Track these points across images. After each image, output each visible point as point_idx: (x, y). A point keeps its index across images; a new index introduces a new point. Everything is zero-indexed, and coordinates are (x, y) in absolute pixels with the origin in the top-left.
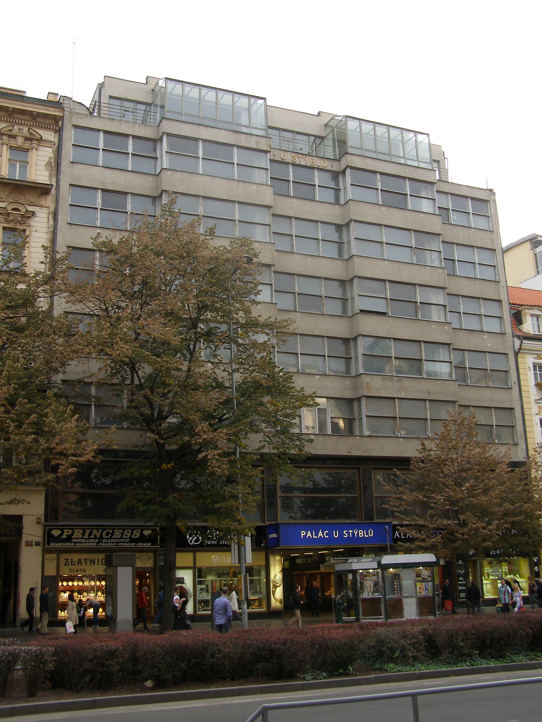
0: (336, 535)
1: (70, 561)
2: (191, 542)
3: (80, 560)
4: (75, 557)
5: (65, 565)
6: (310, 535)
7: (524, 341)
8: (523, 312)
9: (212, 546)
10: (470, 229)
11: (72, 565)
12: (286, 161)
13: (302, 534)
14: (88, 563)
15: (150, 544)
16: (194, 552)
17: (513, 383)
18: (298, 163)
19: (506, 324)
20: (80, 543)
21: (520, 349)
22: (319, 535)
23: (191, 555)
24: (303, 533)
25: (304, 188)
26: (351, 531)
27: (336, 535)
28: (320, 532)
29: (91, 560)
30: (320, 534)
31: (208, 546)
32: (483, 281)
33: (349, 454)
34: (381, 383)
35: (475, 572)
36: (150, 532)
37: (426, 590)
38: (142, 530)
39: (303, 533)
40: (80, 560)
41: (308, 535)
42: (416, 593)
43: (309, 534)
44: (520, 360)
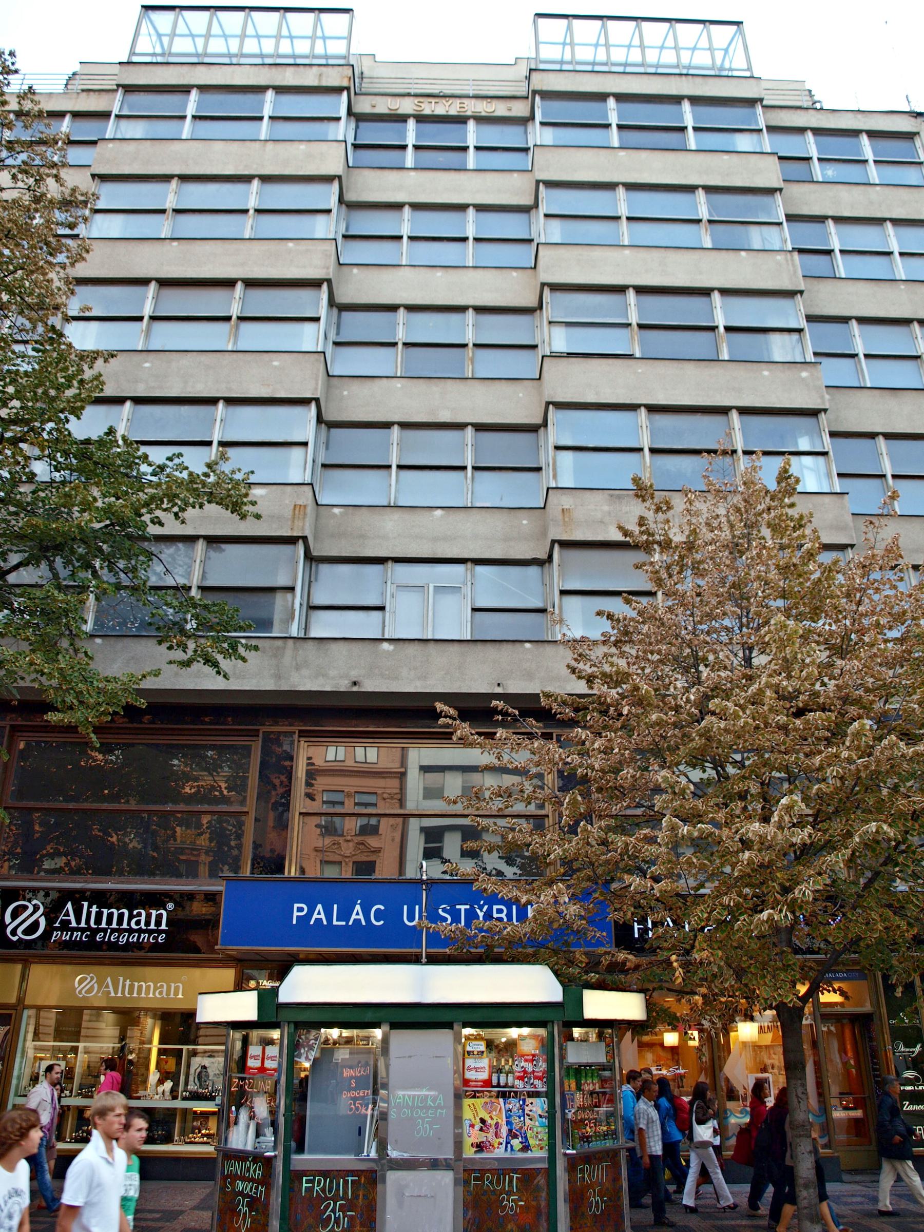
0: (411, 918)
6: (322, 916)
12: (400, 112)
13: (296, 914)
18: (427, 111)
22: (354, 916)
24: (298, 910)
26: (463, 908)
27: (411, 918)
30: (357, 913)
34: (606, 508)
35: (848, 1072)
37: (512, 1134)
39: (300, 910)
41: (315, 916)
42: (458, 1145)
43: (319, 913)
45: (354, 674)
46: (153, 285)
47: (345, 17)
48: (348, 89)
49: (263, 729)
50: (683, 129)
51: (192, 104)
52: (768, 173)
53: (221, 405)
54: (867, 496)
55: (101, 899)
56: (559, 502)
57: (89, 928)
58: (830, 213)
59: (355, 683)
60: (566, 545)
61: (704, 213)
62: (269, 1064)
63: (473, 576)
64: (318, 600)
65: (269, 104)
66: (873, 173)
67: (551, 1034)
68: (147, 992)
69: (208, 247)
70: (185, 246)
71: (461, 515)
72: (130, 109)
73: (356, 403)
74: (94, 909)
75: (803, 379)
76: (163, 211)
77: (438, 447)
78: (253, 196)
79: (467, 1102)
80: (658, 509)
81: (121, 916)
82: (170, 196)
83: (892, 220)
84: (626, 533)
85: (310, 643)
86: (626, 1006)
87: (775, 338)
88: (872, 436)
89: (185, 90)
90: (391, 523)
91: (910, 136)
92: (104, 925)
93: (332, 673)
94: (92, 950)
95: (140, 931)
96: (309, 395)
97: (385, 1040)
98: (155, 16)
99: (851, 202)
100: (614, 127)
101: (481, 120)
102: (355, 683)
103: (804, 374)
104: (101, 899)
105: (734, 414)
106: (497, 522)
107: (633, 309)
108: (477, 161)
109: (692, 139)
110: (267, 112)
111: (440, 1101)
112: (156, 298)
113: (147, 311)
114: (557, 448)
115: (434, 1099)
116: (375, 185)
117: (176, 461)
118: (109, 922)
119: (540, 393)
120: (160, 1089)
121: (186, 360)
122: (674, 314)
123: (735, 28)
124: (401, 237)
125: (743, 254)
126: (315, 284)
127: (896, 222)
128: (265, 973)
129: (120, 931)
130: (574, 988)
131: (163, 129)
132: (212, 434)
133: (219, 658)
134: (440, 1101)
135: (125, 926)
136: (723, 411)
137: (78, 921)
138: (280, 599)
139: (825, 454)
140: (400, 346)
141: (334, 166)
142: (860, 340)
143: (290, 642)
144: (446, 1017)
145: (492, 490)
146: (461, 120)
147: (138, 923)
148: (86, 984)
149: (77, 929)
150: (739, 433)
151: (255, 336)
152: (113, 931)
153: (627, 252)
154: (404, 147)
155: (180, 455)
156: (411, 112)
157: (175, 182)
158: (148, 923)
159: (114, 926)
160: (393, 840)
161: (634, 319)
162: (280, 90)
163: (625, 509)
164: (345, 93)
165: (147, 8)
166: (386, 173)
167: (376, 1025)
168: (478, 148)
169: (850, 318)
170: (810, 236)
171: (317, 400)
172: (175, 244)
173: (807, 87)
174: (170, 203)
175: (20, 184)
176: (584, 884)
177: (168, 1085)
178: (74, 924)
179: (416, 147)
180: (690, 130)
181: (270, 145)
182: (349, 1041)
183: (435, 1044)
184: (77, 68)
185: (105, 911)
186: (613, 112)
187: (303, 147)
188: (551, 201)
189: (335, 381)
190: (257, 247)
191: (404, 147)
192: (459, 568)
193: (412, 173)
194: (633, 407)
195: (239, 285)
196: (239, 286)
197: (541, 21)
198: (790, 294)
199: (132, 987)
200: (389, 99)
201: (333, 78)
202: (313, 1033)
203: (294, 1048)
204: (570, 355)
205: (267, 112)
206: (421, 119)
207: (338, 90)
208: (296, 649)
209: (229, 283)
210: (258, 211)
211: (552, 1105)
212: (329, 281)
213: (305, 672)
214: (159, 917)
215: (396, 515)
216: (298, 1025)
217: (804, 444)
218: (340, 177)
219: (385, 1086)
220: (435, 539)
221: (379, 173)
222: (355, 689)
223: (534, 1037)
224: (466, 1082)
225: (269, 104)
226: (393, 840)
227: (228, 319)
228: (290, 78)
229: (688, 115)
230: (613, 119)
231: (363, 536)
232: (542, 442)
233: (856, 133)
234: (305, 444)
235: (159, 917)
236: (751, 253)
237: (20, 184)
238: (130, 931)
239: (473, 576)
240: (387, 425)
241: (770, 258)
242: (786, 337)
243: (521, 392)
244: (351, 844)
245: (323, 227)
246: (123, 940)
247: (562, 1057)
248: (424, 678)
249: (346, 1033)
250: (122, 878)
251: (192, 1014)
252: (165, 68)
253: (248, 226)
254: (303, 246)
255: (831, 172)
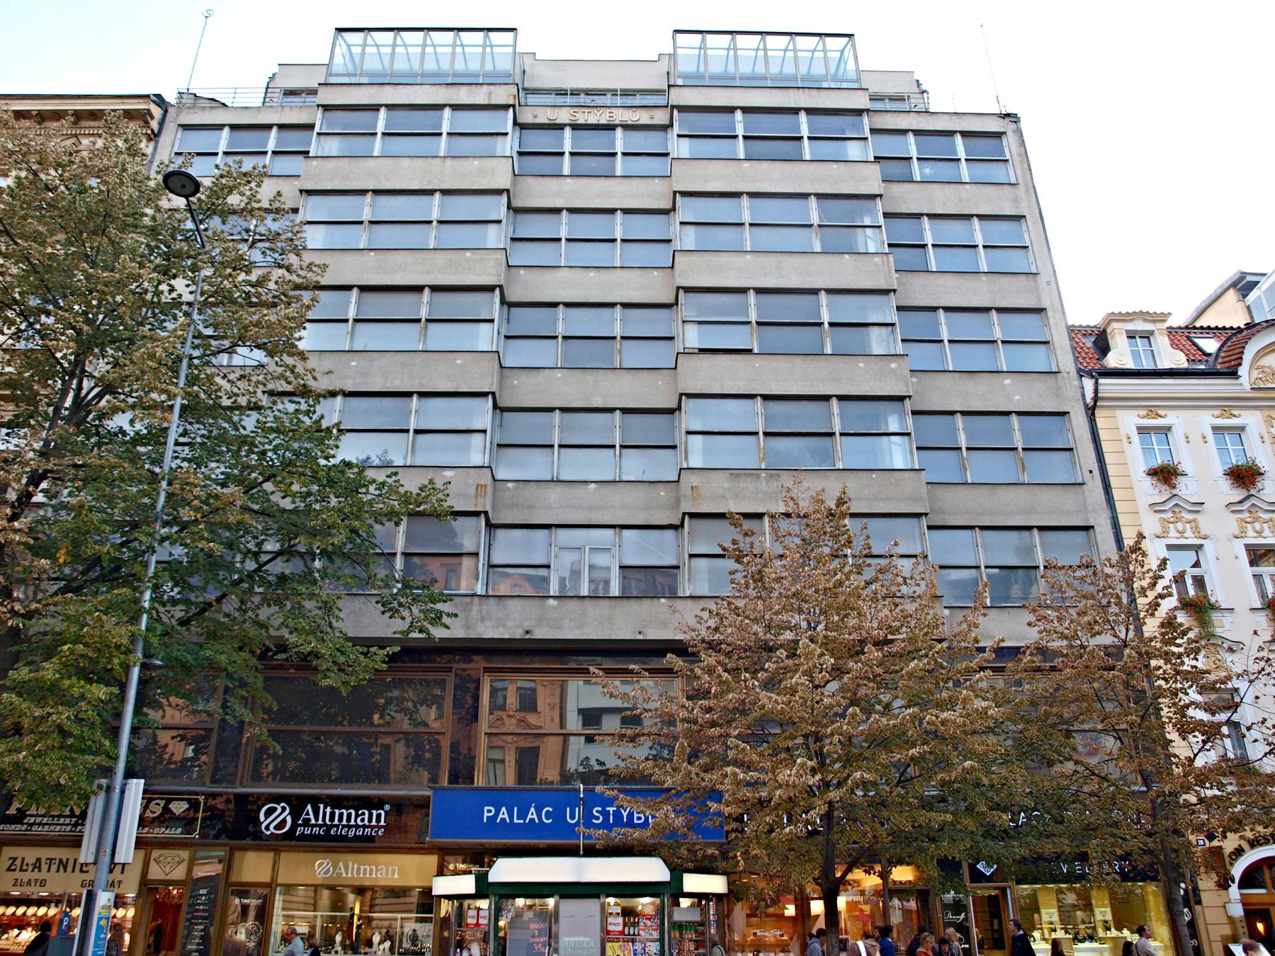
0: (572, 817)
1: (18, 862)
2: (267, 828)
3: (39, 860)
4: (30, 854)
5: (9, 870)
6: (506, 816)
7: (1101, 381)
8: (1109, 331)
9: (313, 838)
10: (960, 187)
11: (21, 870)
12: (558, 122)
13: (486, 814)
14: (54, 868)
15: (179, 830)
16: (277, 851)
17: (1086, 473)
18: (581, 121)
19: (1058, 353)
20: (40, 824)
21: (1096, 399)
22: (530, 816)
23: (268, 857)
25: (594, 163)
27: (572, 817)
28: (532, 810)
29: (61, 861)
30: (532, 814)
31: (303, 837)
32: (996, 277)
33: (640, 637)
34: (727, 485)
36: (185, 806)
38: (169, 801)
39: (489, 811)
40: (39, 860)
41: (501, 816)
44: (1100, 422)
45: (527, 625)
46: (355, 290)
47: (511, 34)
48: (514, 106)
49: (455, 666)
50: (800, 138)
51: (382, 121)
52: (870, 180)
53: (415, 398)
54: (942, 467)
55: (337, 802)
56: (689, 480)
57: (325, 824)
58: (925, 211)
59: (527, 632)
60: (693, 516)
61: (815, 219)
62: (481, 921)
63: (620, 539)
64: (497, 560)
65: (447, 121)
66: (965, 171)
67: (663, 902)
68: (371, 873)
69: (400, 256)
70: (381, 255)
71: (611, 488)
72: (328, 127)
73: (524, 391)
74: (329, 810)
75: (893, 370)
76: (361, 223)
77: (593, 428)
78: (435, 208)
79: (608, 945)
80: (746, 534)
81: (349, 815)
82: (366, 209)
83: (978, 216)
84: (724, 549)
85: (492, 600)
86: (715, 884)
87: (875, 331)
88: (952, 413)
89: (375, 108)
90: (554, 495)
91: (998, 135)
92: (336, 822)
93: (510, 624)
94: (330, 842)
95: (364, 827)
96: (486, 390)
97: (557, 906)
98: (346, 35)
99: (943, 199)
100: (741, 138)
101: (627, 127)
102: (527, 632)
103: (893, 365)
104: (337, 802)
105: (834, 401)
106: (641, 493)
107: (753, 308)
108: (624, 167)
109: (807, 149)
110: (445, 129)
111: (592, 944)
112: (359, 303)
113: (351, 314)
114: (688, 433)
115: (588, 943)
116: (539, 192)
117: (394, 478)
118: (341, 819)
119: (676, 382)
120: (381, 947)
121: (385, 359)
122: (788, 317)
123: (847, 39)
124: (560, 240)
125: (847, 256)
126: (490, 289)
127: (981, 217)
128: (460, 858)
129: (350, 827)
130: (677, 871)
131: (358, 144)
132: (408, 423)
133: (429, 626)
134: (592, 944)
135: (352, 823)
136: (826, 398)
137: (317, 819)
138: (467, 563)
139: (908, 434)
140: (560, 339)
141: (503, 181)
142: (945, 327)
143: (476, 599)
144: (594, 891)
145: (635, 465)
146: (611, 128)
147: (363, 820)
148: (321, 867)
149: (316, 825)
150: (836, 417)
151: (441, 336)
152: (344, 826)
153: (749, 257)
154: (562, 154)
155: (396, 474)
156: (567, 121)
157: (369, 195)
158: (370, 820)
159: (344, 822)
160: (552, 720)
161: (753, 317)
162: (456, 107)
163: (742, 485)
164: (511, 110)
165: (340, 30)
166: (547, 180)
167: (552, 896)
168: (624, 154)
169: (938, 308)
170: (904, 231)
171: (493, 394)
172: (372, 254)
173: (916, 77)
174: (366, 215)
175: (268, 258)
176: (689, 802)
177: (388, 944)
178: (313, 822)
179: (572, 154)
180: (805, 139)
181: (449, 161)
182: (530, 907)
183: (590, 907)
184: (276, 69)
185: (337, 812)
186: (739, 124)
187: (476, 162)
188: (688, 209)
189: (507, 372)
190: (440, 255)
191: (562, 154)
192: (610, 532)
193: (569, 180)
194: (751, 397)
195: (427, 290)
196: (427, 290)
197: (679, 36)
198: (886, 292)
199: (359, 869)
200: (549, 110)
201: (502, 95)
202: (510, 901)
203: (498, 912)
204: (702, 351)
205: (445, 129)
206: (576, 127)
207: (506, 107)
208: (480, 604)
209: (418, 289)
210: (440, 222)
211: (662, 946)
212: (501, 287)
213: (488, 623)
214: (379, 816)
215: (559, 489)
216: (502, 896)
217: (893, 426)
218: (508, 191)
219: (557, 936)
220: (590, 509)
221: (541, 180)
222: (528, 637)
223: (653, 903)
224: (608, 932)
225: (447, 121)
226: (552, 720)
227: (419, 321)
228: (463, 96)
229: (804, 125)
230: (740, 131)
231: (531, 507)
232: (677, 424)
233: (951, 133)
234: (485, 431)
235: (379, 816)
236: (855, 256)
237: (268, 258)
238: (357, 827)
239: (620, 539)
240: (551, 410)
241: (869, 256)
242: (883, 329)
243: (660, 380)
244: (514, 721)
245: (495, 238)
246: (351, 833)
247: (670, 916)
248: (581, 627)
249: (529, 902)
250: (350, 785)
251: (430, 889)
252: (357, 88)
253: (431, 237)
254: (478, 255)
255: (929, 170)
